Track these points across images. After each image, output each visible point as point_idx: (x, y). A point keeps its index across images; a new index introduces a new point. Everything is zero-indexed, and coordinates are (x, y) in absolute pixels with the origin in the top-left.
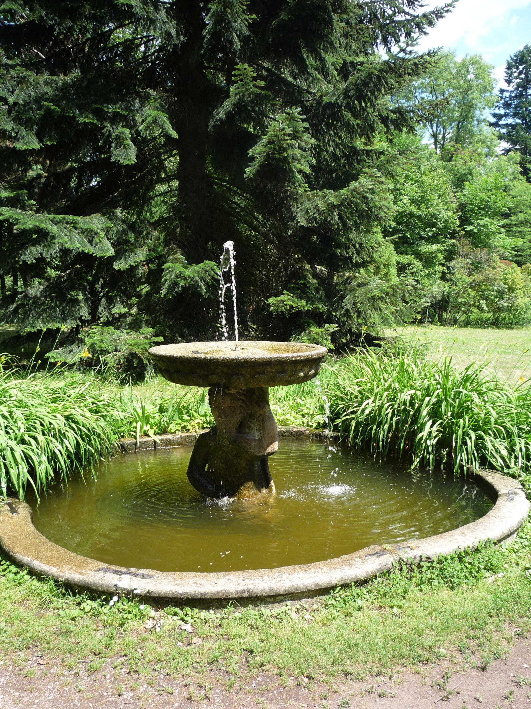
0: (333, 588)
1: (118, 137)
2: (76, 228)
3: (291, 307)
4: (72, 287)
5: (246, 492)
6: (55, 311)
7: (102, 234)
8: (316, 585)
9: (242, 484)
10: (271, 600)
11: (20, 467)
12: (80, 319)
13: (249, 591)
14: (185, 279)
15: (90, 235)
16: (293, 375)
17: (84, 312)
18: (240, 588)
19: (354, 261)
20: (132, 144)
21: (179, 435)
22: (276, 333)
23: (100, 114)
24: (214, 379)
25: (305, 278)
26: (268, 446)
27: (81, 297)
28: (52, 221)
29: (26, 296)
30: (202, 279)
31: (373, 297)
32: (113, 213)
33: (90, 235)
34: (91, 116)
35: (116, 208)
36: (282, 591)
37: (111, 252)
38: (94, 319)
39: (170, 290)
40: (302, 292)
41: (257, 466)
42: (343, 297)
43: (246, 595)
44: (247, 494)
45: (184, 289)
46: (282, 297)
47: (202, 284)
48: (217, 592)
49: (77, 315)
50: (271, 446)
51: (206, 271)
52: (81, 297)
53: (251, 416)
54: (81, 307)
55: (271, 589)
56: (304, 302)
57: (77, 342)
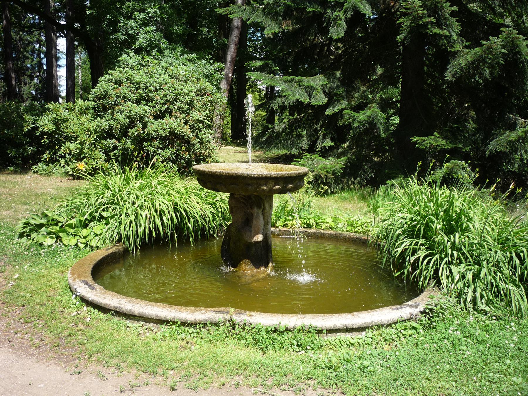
0: (174, 323)
1: (335, 19)
2: (300, 86)
5: (243, 266)
6: (287, 142)
7: (319, 89)
8: (157, 316)
9: (241, 260)
10: (133, 318)
11: (134, 229)
12: (301, 148)
13: (119, 308)
15: (309, 91)
16: (258, 187)
17: (305, 144)
18: (117, 305)
26: (254, 237)
32: (334, 74)
33: (309, 91)
34: (316, 6)
35: (337, 70)
36: (136, 313)
37: (325, 100)
38: (312, 150)
43: (118, 310)
44: (244, 267)
48: (107, 304)
49: (300, 146)
50: (256, 237)
54: (304, 140)
55: (131, 310)
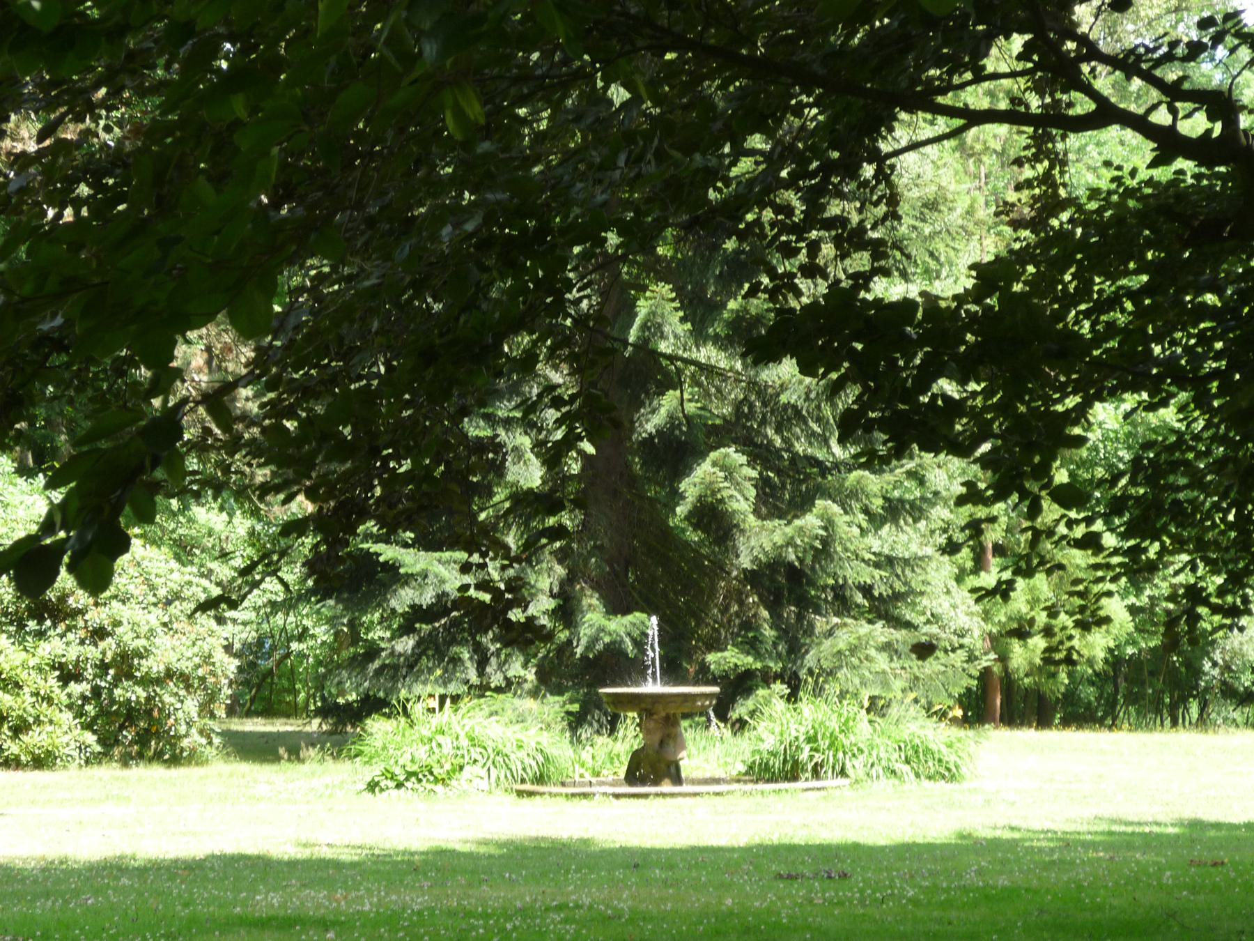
3: (736, 665)
4: (453, 641)
14: (610, 634)
19: (876, 594)
20: (532, 457)
21: (611, 778)
22: (408, 404)
23: (490, 419)
24: (643, 706)
25: (757, 628)
27: (466, 656)
28: (439, 561)
29: (392, 653)
30: (629, 634)
31: (839, 652)
39: (588, 648)
40: (752, 646)
41: (673, 770)
42: (807, 652)
45: (607, 646)
46: (726, 654)
47: (627, 640)
51: (635, 625)
52: (466, 656)
53: (669, 736)
56: (750, 659)
57: (1015, 497)
